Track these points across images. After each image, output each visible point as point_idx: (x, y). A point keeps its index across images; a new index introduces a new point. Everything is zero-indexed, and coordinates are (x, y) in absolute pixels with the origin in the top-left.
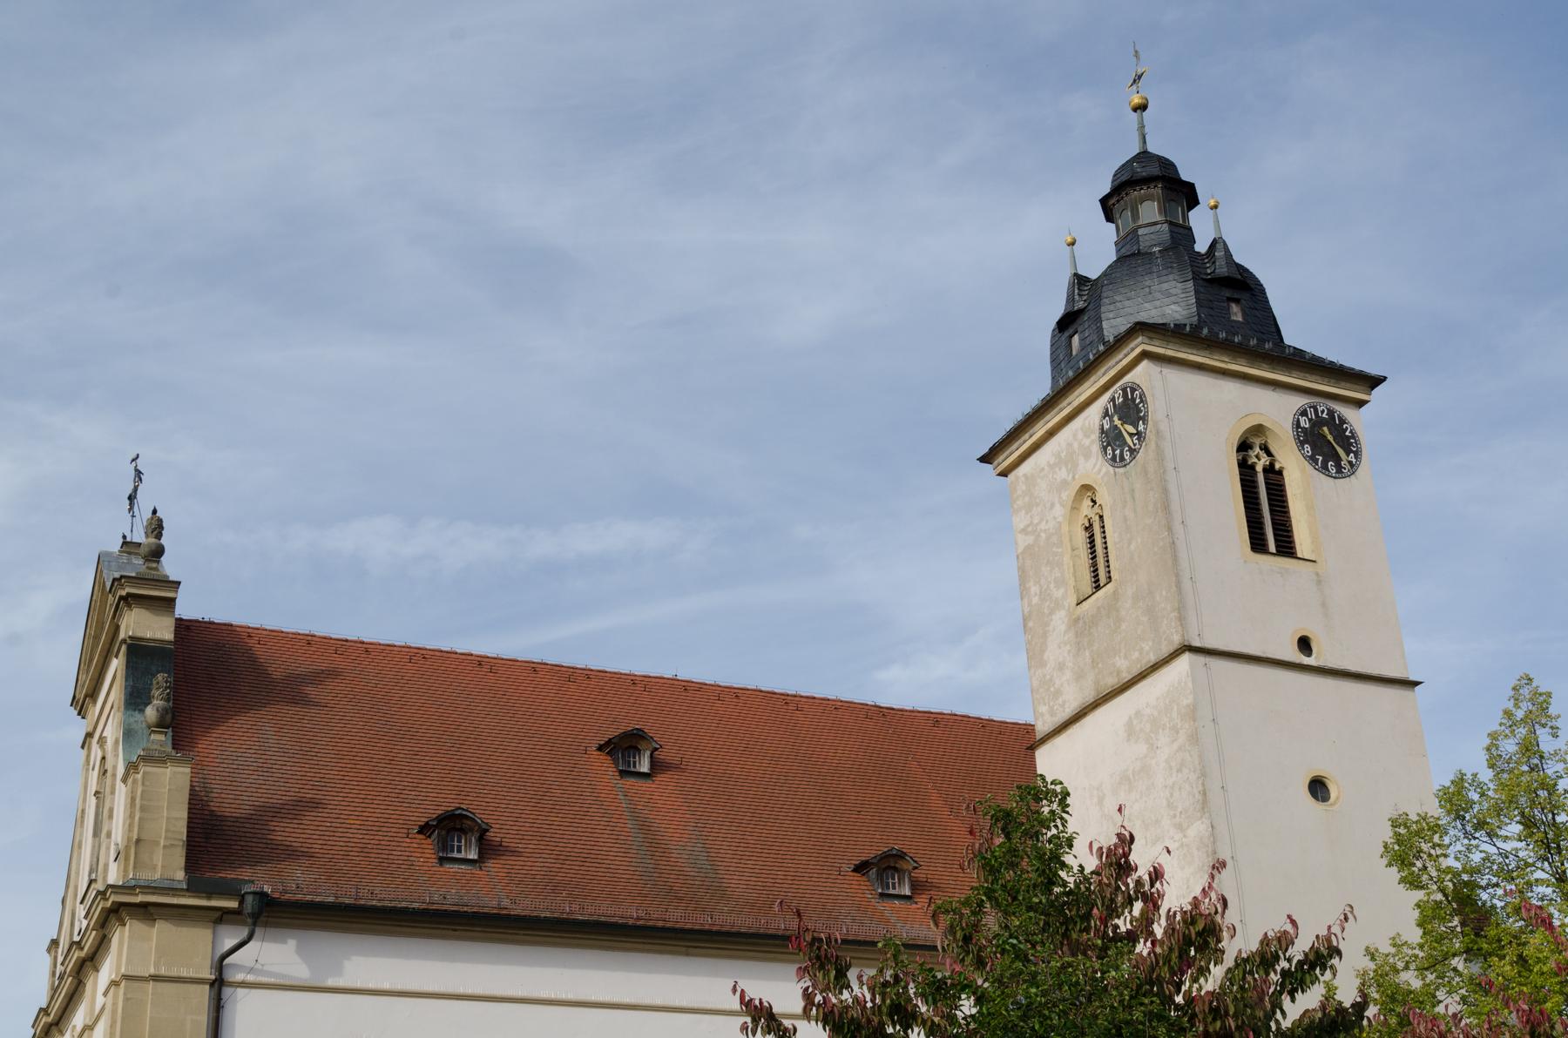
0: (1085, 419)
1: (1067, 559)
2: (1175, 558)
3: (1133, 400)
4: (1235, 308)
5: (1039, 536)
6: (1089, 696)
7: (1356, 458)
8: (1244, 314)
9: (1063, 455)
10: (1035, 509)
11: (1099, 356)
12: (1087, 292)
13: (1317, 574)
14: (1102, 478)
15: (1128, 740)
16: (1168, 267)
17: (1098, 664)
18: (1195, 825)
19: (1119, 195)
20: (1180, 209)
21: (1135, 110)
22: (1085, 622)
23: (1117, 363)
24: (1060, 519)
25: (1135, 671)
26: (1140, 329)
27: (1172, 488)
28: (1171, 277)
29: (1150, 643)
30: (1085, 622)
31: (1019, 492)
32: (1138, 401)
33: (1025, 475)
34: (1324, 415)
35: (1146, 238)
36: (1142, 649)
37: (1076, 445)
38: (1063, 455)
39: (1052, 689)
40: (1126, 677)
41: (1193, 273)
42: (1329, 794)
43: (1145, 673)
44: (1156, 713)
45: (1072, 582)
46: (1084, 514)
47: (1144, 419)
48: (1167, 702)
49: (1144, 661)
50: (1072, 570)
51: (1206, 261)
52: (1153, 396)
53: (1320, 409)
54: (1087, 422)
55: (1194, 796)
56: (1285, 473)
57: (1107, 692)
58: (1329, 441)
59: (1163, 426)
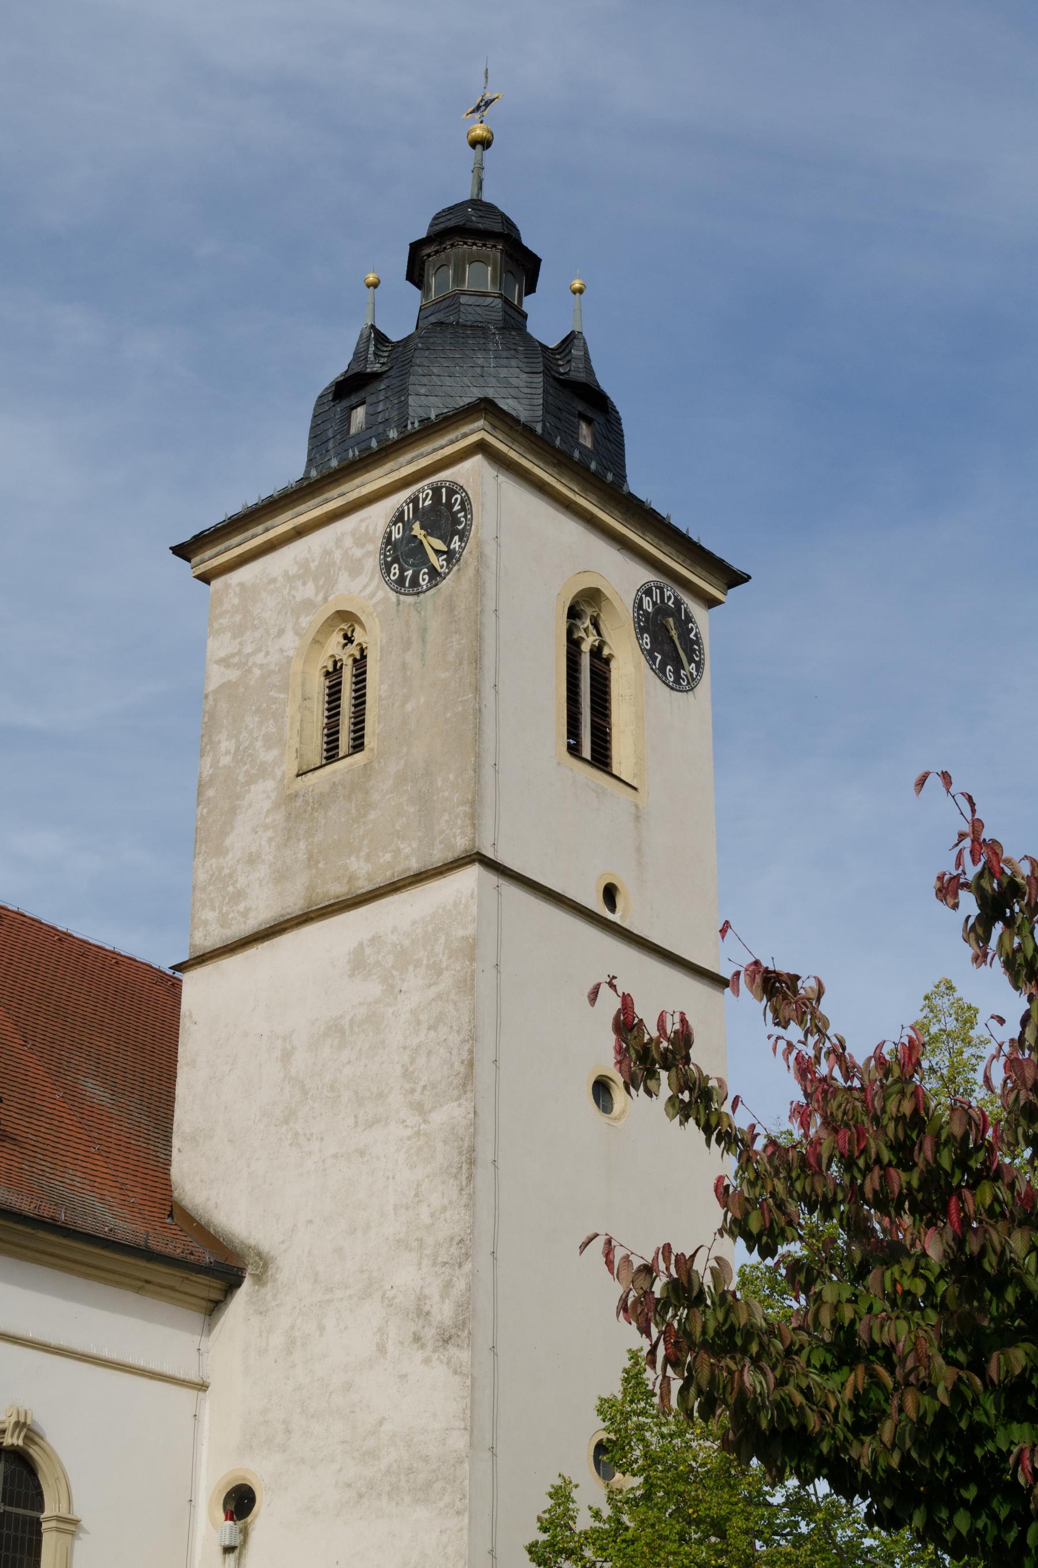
0: (362, 521)
1: (291, 710)
2: (478, 732)
3: (450, 505)
4: (584, 429)
5: (249, 671)
6: (294, 904)
7: (697, 670)
8: (595, 441)
9: (313, 566)
10: (249, 633)
11: (309, 485)
12: (386, 354)
13: (637, 807)
14: (375, 606)
15: (352, 976)
16: (510, 349)
17: (318, 862)
18: (445, 1108)
19: (440, 244)
20: (517, 287)
21: (474, 144)
22: (306, 802)
23: (435, 450)
24: (291, 653)
25: (381, 879)
26: (485, 409)
27: (489, 634)
28: (514, 362)
29: (415, 845)
30: (306, 802)
31: (226, 606)
32: (457, 508)
33: (242, 585)
34: (670, 603)
35: (470, 309)
36: (397, 852)
38: (313, 566)
39: (230, 889)
40: (364, 886)
41: (545, 366)
42: (612, 1105)
43: (400, 884)
44: (407, 943)
45: (294, 743)
46: (331, 653)
47: (463, 536)
48: (430, 928)
49: (398, 869)
50: (297, 726)
51: (558, 357)
52: (483, 505)
53: (667, 594)
54: (364, 525)
55: (452, 1066)
56: (613, 665)
57: (327, 903)
58: (671, 638)
59: (489, 550)
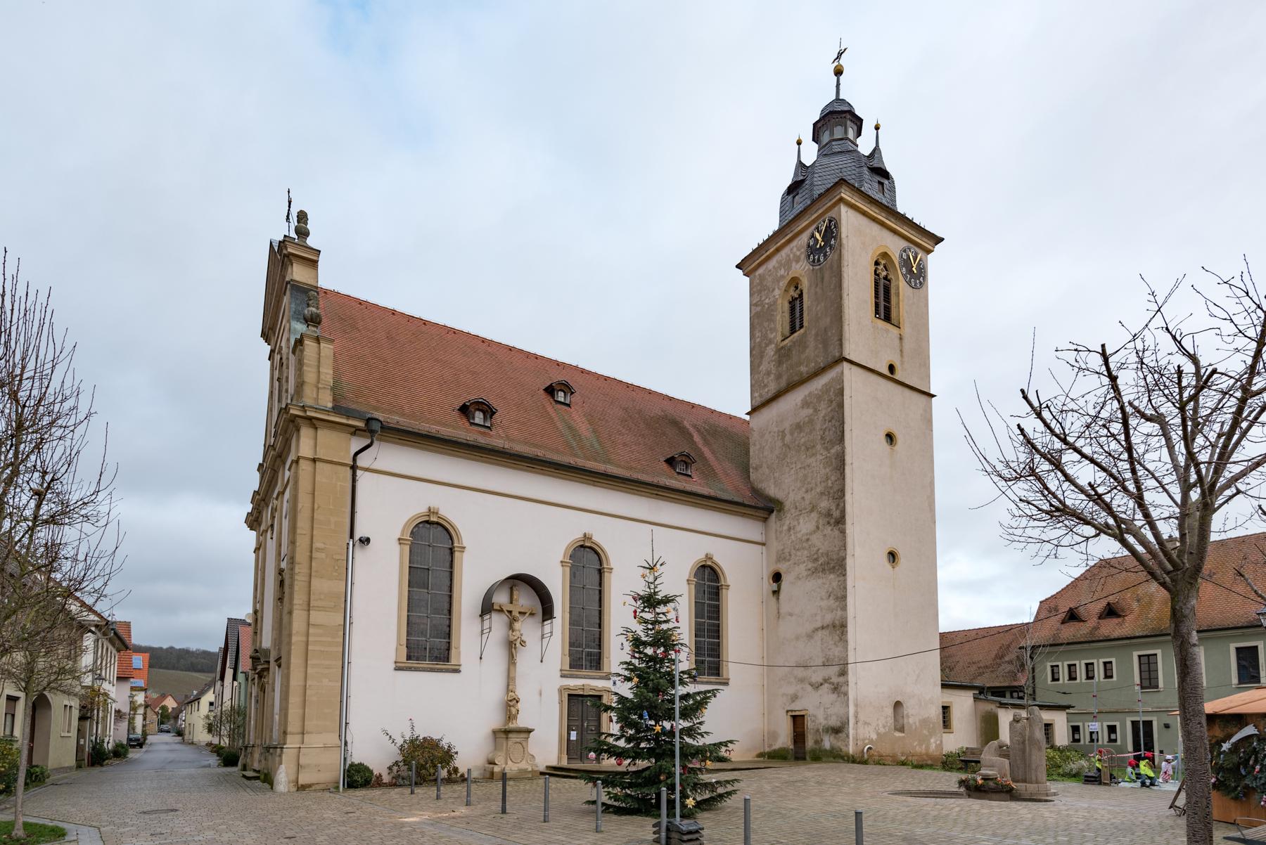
5: (764, 306)
9: (783, 262)
13: (900, 335)
14: (805, 272)
29: (822, 358)
32: (833, 227)
33: (759, 275)
37: (791, 256)
44: (820, 393)
50: (781, 323)
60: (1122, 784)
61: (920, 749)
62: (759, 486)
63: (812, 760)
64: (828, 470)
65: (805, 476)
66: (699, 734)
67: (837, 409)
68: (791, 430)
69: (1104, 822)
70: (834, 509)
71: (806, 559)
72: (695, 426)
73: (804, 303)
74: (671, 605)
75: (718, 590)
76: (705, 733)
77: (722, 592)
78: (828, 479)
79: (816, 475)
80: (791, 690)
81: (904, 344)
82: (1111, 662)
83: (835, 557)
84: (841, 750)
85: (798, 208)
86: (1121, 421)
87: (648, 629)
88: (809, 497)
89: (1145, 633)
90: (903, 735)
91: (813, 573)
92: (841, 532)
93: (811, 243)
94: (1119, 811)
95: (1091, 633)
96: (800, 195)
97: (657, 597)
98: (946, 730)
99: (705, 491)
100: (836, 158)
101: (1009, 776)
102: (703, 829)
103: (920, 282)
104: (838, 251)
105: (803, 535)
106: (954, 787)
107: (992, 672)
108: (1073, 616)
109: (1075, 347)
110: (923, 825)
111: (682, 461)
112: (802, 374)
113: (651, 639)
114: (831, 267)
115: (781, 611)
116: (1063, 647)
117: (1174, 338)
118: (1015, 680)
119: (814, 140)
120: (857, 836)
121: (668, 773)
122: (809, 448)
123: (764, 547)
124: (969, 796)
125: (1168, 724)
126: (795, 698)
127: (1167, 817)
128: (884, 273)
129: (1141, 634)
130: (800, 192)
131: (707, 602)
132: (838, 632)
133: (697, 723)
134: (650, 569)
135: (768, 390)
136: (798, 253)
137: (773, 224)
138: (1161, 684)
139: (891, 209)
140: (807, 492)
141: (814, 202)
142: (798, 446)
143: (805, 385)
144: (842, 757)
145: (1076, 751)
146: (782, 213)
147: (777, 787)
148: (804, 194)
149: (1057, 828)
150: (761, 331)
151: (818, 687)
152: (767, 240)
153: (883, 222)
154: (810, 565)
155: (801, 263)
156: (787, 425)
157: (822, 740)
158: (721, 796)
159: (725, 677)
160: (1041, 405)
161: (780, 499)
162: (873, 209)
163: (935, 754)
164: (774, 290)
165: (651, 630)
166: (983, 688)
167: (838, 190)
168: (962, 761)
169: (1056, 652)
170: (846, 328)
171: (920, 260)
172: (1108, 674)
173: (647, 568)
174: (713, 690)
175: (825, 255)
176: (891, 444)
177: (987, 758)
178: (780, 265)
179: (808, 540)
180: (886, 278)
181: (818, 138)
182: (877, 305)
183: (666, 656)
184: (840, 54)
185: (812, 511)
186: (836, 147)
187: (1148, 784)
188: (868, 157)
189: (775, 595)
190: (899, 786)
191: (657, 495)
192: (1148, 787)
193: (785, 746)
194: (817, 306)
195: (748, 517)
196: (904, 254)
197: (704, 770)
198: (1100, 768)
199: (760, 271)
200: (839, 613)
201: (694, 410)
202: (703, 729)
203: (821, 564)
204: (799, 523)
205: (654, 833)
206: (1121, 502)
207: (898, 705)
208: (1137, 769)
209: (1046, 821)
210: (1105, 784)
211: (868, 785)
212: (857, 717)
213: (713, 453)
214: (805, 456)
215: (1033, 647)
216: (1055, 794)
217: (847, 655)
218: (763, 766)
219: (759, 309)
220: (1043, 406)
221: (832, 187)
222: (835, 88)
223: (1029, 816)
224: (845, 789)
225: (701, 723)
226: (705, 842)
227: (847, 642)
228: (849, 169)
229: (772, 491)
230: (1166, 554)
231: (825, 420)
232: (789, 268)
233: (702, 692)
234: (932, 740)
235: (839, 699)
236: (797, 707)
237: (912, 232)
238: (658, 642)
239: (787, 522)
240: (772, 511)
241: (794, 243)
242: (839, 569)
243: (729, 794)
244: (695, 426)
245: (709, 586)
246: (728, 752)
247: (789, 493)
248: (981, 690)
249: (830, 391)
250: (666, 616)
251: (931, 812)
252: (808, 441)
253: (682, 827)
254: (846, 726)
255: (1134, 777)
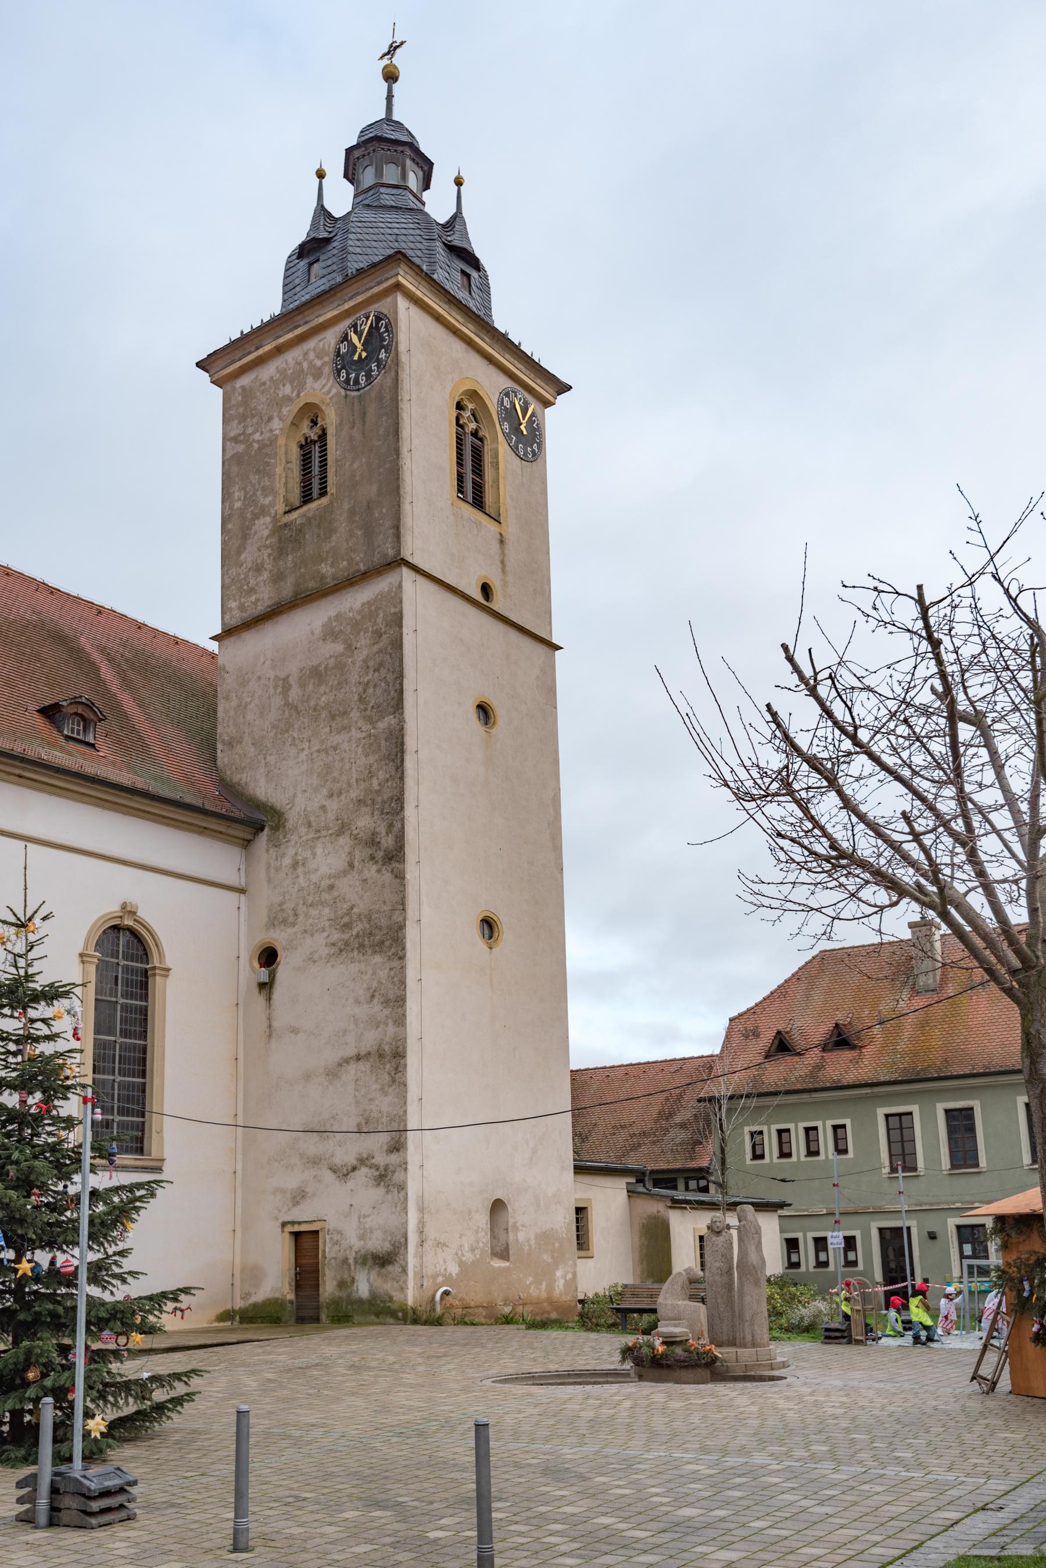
5: (251, 445)
13: (501, 535)
14: (331, 399)
32: (383, 330)
33: (243, 388)
37: (305, 365)
44: (359, 617)
50: (284, 480)
60: (884, 1340)
61: (537, 1291)
62: (236, 779)
63: (333, 1321)
64: (372, 759)
65: (328, 767)
66: (115, 1276)
67: (389, 650)
68: (300, 678)
69: (876, 1412)
70: (384, 833)
71: (327, 924)
72: (102, 650)
73: (329, 452)
74: (61, 1005)
75: (147, 977)
76: (130, 1273)
77: (154, 981)
78: (371, 775)
79: (348, 766)
80: (291, 1181)
81: (506, 552)
82: (844, 1126)
83: (384, 922)
84: (391, 1299)
85: (318, 286)
86: (945, 714)
87: (8, 1052)
88: (336, 807)
89: (894, 1077)
90: (507, 1264)
91: (341, 951)
92: (396, 877)
93: (343, 350)
94: (894, 1390)
95: (812, 1075)
96: (321, 264)
97: (31, 985)
98: (583, 1253)
99: (124, 778)
100: (388, 216)
101: (706, 1335)
102: (134, 1483)
103: (533, 451)
104: (393, 373)
105: (322, 878)
106: (613, 1361)
107: (654, 1143)
108: (782, 1046)
109: (876, 583)
110: (573, 1440)
111: (76, 714)
112: (323, 577)
113: (14, 1074)
114: (380, 398)
115: (276, 1024)
116: (779, 1098)
117: (1007, 591)
118: (692, 1159)
119: (346, 176)
120: (478, 1473)
121: (44, 1365)
122: (337, 715)
123: (242, 896)
124: (641, 1378)
125: (934, 1233)
126: (299, 1196)
127: (969, 1396)
128: (473, 426)
129: (887, 1078)
130: (322, 258)
131: (121, 1001)
132: (388, 1066)
133: (115, 1254)
134: (17, 926)
135: (257, 600)
136: (318, 363)
137: (272, 305)
138: (921, 1164)
139: (483, 320)
140: (331, 796)
141: (348, 280)
142: (315, 710)
143: (330, 598)
144: (393, 1314)
145: (805, 1285)
146: (288, 287)
147: (270, 1380)
148: (330, 262)
149: (804, 1428)
150: (244, 489)
151: (346, 1175)
152: (259, 328)
153: (471, 339)
154: (336, 936)
155: (323, 381)
156: (293, 668)
157: (353, 1280)
158: (160, 1408)
159: (154, 1155)
160: (816, 674)
161: (278, 806)
162: (454, 314)
163: (564, 1298)
164: (270, 419)
165: (15, 1054)
166: (643, 1173)
167: (392, 269)
168: (618, 1310)
169: (768, 1107)
170: (406, 508)
171: (533, 415)
172: (841, 1147)
173: (12, 924)
174: (149, 1182)
175: (368, 376)
176: (486, 724)
177: (669, 1302)
178: (284, 377)
179: (331, 887)
180: (475, 434)
181: (354, 174)
182: (460, 478)
183: (49, 1111)
184: (393, 49)
185: (340, 833)
186: (387, 197)
187: (923, 1338)
188: (443, 226)
189: (264, 992)
190: (512, 1367)
191: (20, 776)
192: (924, 1344)
193: (278, 1295)
194: (353, 462)
195: (213, 837)
196: (506, 399)
197: (125, 1354)
198: (849, 1312)
199: (245, 381)
200: (391, 1029)
201: (101, 619)
202: (127, 1264)
203: (357, 936)
204: (314, 855)
205: (20, 1501)
206: (944, 850)
207: (498, 1206)
208: (903, 1313)
209: (783, 1416)
210: (858, 1342)
211: (451, 1366)
212: (422, 1232)
213: (141, 705)
214: (327, 729)
215: (731, 1098)
216: (784, 1365)
217: (405, 1111)
218: (234, 1338)
219: (241, 448)
220: (819, 677)
221: (381, 262)
222: (385, 101)
223: (754, 1408)
224: (409, 1378)
225: (122, 1253)
226: (138, 1511)
227: (405, 1085)
228: (411, 238)
229: (262, 789)
230: (1012, 942)
231: (368, 668)
232: (301, 386)
233: (124, 1187)
234: (559, 1273)
235: (389, 1197)
236: (304, 1214)
237: (520, 366)
238: (30, 1080)
239: (291, 852)
240: (262, 829)
241: (311, 344)
242: (391, 946)
243: (178, 1401)
244: (102, 650)
245: (126, 969)
246: (179, 1313)
247: (295, 795)
248: (640, 1176)
249: (378, 615)
250: (49, 1025)
251: (582, 1414)
252: (335, 701)
253: (86, 1482)
254: (402, 1251)
255: (900, 1327)
